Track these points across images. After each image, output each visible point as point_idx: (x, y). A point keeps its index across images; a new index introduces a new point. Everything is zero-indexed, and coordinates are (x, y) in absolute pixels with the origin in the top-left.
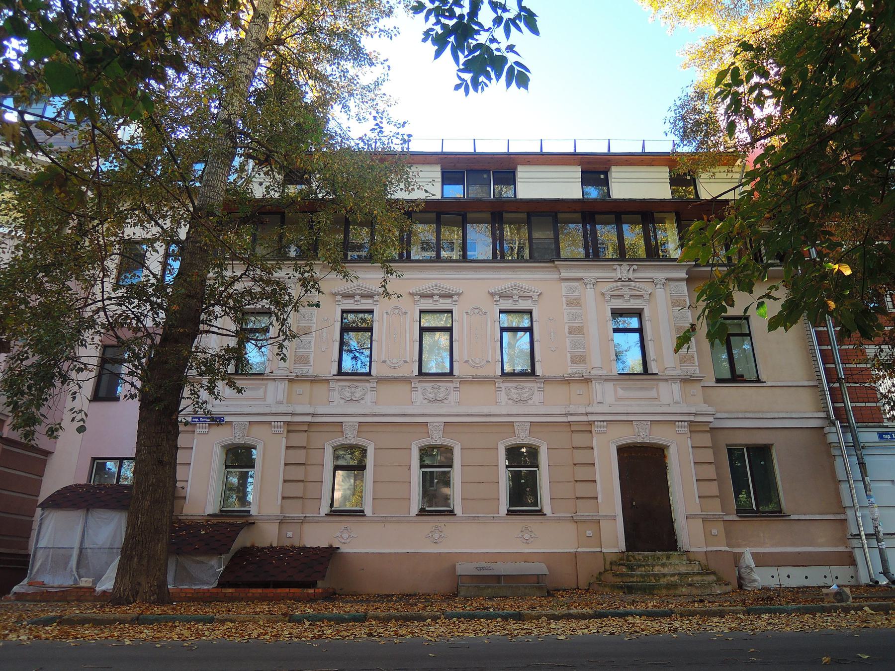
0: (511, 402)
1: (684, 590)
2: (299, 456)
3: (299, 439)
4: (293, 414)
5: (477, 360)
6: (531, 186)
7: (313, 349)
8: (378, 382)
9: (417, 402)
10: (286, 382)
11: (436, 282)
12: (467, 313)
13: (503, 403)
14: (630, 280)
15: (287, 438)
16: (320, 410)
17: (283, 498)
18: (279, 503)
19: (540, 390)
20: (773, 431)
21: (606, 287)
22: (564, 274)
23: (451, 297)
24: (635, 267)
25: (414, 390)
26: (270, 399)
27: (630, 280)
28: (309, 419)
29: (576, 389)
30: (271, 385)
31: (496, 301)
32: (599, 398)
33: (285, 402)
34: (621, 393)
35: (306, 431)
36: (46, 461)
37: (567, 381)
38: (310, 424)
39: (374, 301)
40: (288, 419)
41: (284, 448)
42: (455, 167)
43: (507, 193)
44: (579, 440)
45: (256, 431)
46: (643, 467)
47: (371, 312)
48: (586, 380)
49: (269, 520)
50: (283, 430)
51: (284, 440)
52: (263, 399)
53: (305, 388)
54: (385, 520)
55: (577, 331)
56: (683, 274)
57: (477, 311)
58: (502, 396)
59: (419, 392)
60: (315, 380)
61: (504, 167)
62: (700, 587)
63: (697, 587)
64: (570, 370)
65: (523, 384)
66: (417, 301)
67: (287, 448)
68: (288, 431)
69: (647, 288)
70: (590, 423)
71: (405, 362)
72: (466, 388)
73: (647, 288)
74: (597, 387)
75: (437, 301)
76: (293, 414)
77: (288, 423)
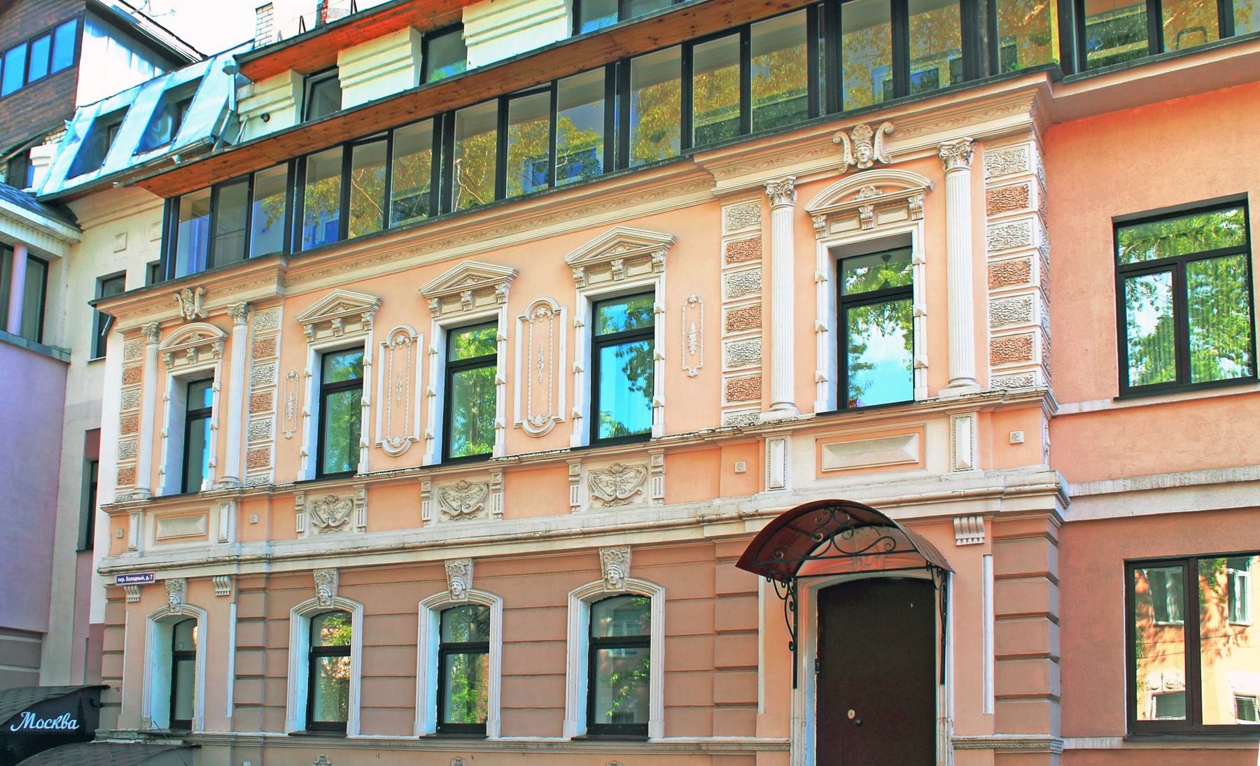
2: (255, 634)
3: (255, 604)
5: (538, 421)
7: (273, 438)
9: (580, 509)
11: (466, 263)
12: (523, 320)
13: (584, 508)
14: (877, 164)
16: (279, 551)
20: (1127, 528)
21: (816, 199)
23: (648, 257)
24: (887, 127)
26: (937, 462)
27: (877, 164)
28: (263, 568)
29: (737, 461)
30: (936, 431)
31: (579, 280)
33: (231, 540)
34: (162, 531)
35: (264, 589)
36: (40, 645)
38: (269, 576)
39: (909, 211)
40: (233, 569)
47: (360, 347)
51: (233, 607)
52: (204, 537)
53: (259, 513)
55: (747, 319)
56: (1022, 117)
57: (542, 311)
58: (582, 493)
59: (585, 483)
60: (274, 495)
64: (728, 416)
65: (624, 462)
66: (820, 230)
67: (240, 620)
69: (919, 176)
71: (413, 441)
73: (919, 176)
75: (466, 304)
77: (236, 578)
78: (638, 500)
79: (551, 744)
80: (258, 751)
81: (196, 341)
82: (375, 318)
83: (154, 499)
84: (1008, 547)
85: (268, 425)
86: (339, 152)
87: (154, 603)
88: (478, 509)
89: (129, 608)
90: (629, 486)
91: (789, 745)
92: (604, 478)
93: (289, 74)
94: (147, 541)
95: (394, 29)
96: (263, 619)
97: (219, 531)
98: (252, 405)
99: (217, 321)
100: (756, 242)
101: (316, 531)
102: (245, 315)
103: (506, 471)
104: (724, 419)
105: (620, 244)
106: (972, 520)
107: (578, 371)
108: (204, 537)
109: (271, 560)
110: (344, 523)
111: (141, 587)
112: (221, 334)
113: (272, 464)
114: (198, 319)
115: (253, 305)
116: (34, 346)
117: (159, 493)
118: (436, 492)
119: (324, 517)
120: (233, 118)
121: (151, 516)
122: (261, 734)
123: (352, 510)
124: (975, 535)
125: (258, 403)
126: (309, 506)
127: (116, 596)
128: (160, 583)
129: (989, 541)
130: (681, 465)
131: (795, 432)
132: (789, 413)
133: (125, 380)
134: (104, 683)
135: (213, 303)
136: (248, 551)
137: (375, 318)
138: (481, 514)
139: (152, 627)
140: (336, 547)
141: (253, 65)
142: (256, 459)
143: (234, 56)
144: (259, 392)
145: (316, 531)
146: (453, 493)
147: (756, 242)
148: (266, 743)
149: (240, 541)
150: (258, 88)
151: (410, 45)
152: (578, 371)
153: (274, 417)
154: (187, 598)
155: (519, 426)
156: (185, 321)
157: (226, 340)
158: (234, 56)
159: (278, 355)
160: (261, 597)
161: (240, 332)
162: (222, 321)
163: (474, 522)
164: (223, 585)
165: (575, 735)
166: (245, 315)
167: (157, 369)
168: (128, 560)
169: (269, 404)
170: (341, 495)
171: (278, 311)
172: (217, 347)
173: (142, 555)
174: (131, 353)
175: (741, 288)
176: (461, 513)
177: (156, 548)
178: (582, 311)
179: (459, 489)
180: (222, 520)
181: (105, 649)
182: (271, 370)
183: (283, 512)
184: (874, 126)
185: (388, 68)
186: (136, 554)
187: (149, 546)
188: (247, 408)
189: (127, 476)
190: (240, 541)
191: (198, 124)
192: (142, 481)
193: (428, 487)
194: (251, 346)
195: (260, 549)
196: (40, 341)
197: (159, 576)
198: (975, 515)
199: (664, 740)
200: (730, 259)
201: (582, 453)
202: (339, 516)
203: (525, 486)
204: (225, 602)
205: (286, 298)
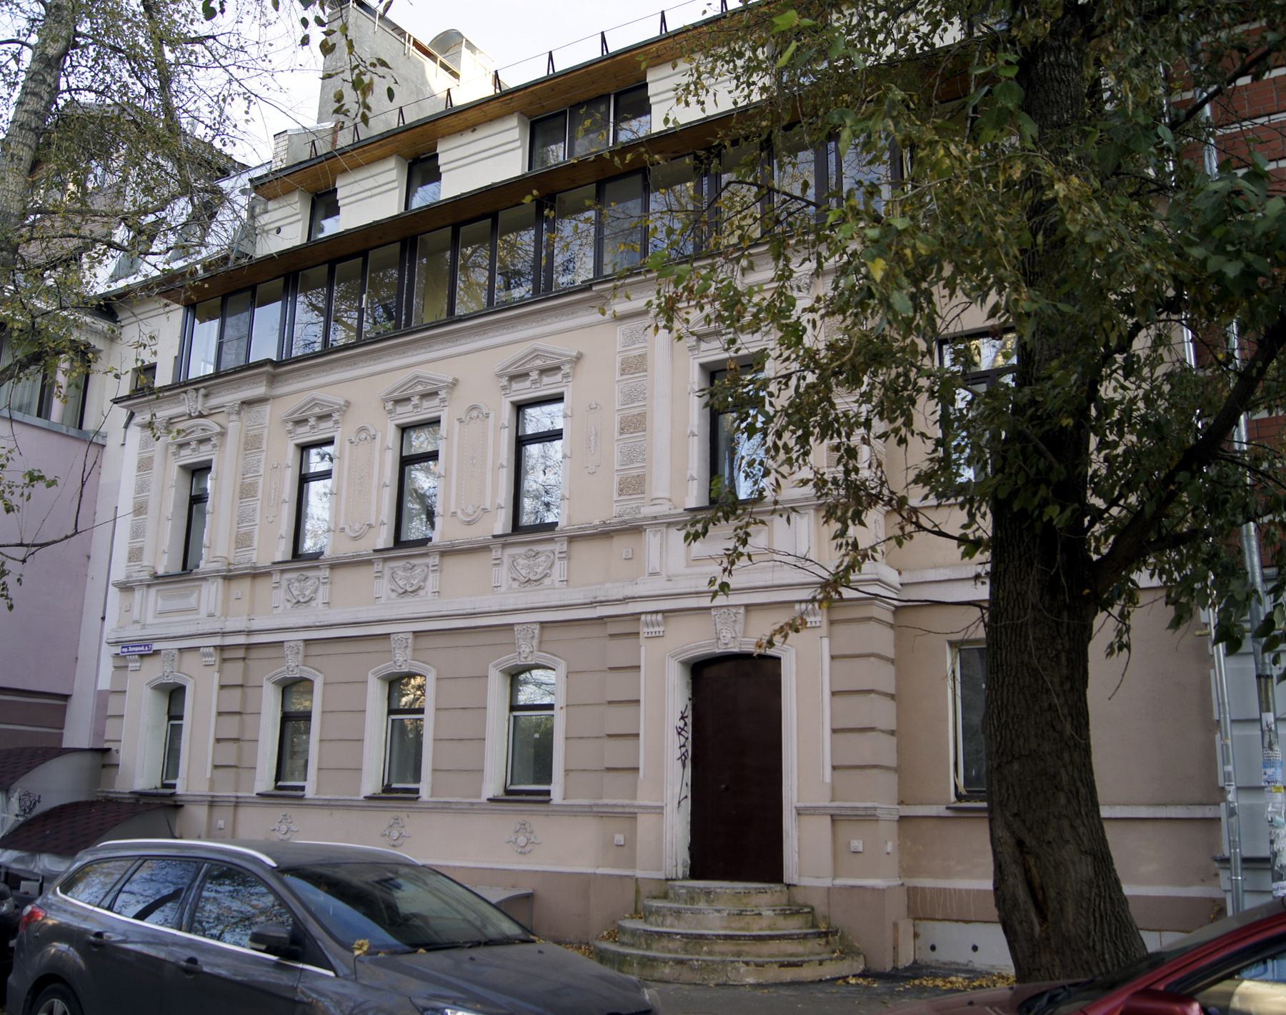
0: (515, 585)
1: (667, 970)
3: (235, 672)
4: (224, 634)
5: (470, 511)
6: (670, 105)
8: (333, 567)
10: (220, 581)
11: (315, 394)
12: (461, 421)
15: (830, 636)
16: (256, 625)
17: (216, 767)
18: (828, 779)
19: (566, 556)
22: (621, 306)
25: (498, 563)
28: (241, 640)
29: (621, 545)
32: (654, 564)
34: (162, 605)
35: (244, 659)
36: (65, 706)
37: (606, 533)
38: (249, 647)
40: (217, 641)
41: (216, 687)
42: (549, 106)
43: (636, 129)
44: (618, 652)
45: (191, 661)
46: (733, 709)
48: (634, 529)
49: (197, 800)
50: (214, 659)
52: (195, 610)
54: (445, 807)
55: (634, 424)
57: (474, 413)
58: (503, 574)
60: (256, 574)
61: (615, 82)
62: (700, 968)
63: (692, 969)
65: (414, 561)
68: (832, 623)
70: (636, 616)
71: (370, 526)
72: (452, 564)
74: (652, 540)
75: (313, 427)
76: (224, 634)
77: (222, 648)
78: (547, 581)
79: (472, 804)
80: (232, 809)
81: (199, 434)
82: (573, 368)
83: (156, 577)
84: (840, 629)
85: (254, 510)
86: (325, 268)
87: (155, 671)
88: (420, 588)
89: (130, 674)
90: (539, 570)
91: (662, 808)
92: (521, 561)
93: (296, 197)
94: (151, 614)
95: (383, 158)
96: (242, 686)
97: (207, 607)
98: (241, 492)
99: (213, 418)
100: (642, 358)
101: (289, 605)
102: (238, 413)
103: (572, 539)
104: (616, 510)
105: (537, 357)
106: (654, 617)
107: (502, 466)
108: (195, 610)
109: (250, 633)
110: (311, 599)
111: (142, 656)
112: (218, 429)
113: (255, 545)
114: (201, 416)
115: (247, 403)
116: (73, 432)
117: (161, 571)
118: (387, 573)
119: (296, 593)
120: (250, 231)
121: (153, 591)
122: (233, 794)
123: (553, 564)
124: (657, 629)
125: (247, 491)
126: (284, 584)
127: (121, 666)
128: (157, 652)
129: (825, 624)
130: (580, 549)
131: (669, 525)
132: (663, 509)
133: (139, 469)
134: (106, 746)
135: (214, 402)
136: (230, 626)
137: (573, 368)
138: (422, 593)
139: (950, 661)
140: (302, 622)
141: (269, 187)
142: (243, 541)
143: (251, 180)
144: (248, 481)
145: (289, 605)
146: (400, 573)
147: (642, 358)
148: (237, 803)
149: (226, 614)
150: (271, 205)
151: (395, 172)
152: (502, 466)
153: (259, 503)
154: (745, 631)
155: (454, 514)
156: (191, 417)
157: (222, 434)
158: (251, 180)
159: (264, 447)
160: (240, 664)
161: (234, 426)
162: (219, 418)
163: (417, 599)
164: (210, 655)
165: (491, 796)
166: (238, 413)
167: (166, 458)
168: (133, 633)
169: (256, 491)
170: (310, 574)
171: (267, 409)
172: (214, 441)
173: (144, 627)
174: (144, 445)
175: (630, 397)
176: (406, 592)
177: (156, 621)
178: (392, 436)
179: (405, 569)
180: (210, 595)
181: (109, 713)
182: (259, 461)
183: (263, 586)
184: (197, 390)
185: (372, 193)
186: (138, 626)
187: (150, 619)
188: (237, 494)
189: (135, 555)
190: (226, 614)
191: (219, 239)
192: (147, 561)
193: (499, 554)
194: (243, 440)
195: (241, 624)
196: (80, 427)
197: (156, 646)
198: (657, 612)
199: (565, 802)
200: (623, 372)
201: (502, 540)
202: (307, 593)
203: (346, 578)
204: (210, 669)
205: (274, 398)
